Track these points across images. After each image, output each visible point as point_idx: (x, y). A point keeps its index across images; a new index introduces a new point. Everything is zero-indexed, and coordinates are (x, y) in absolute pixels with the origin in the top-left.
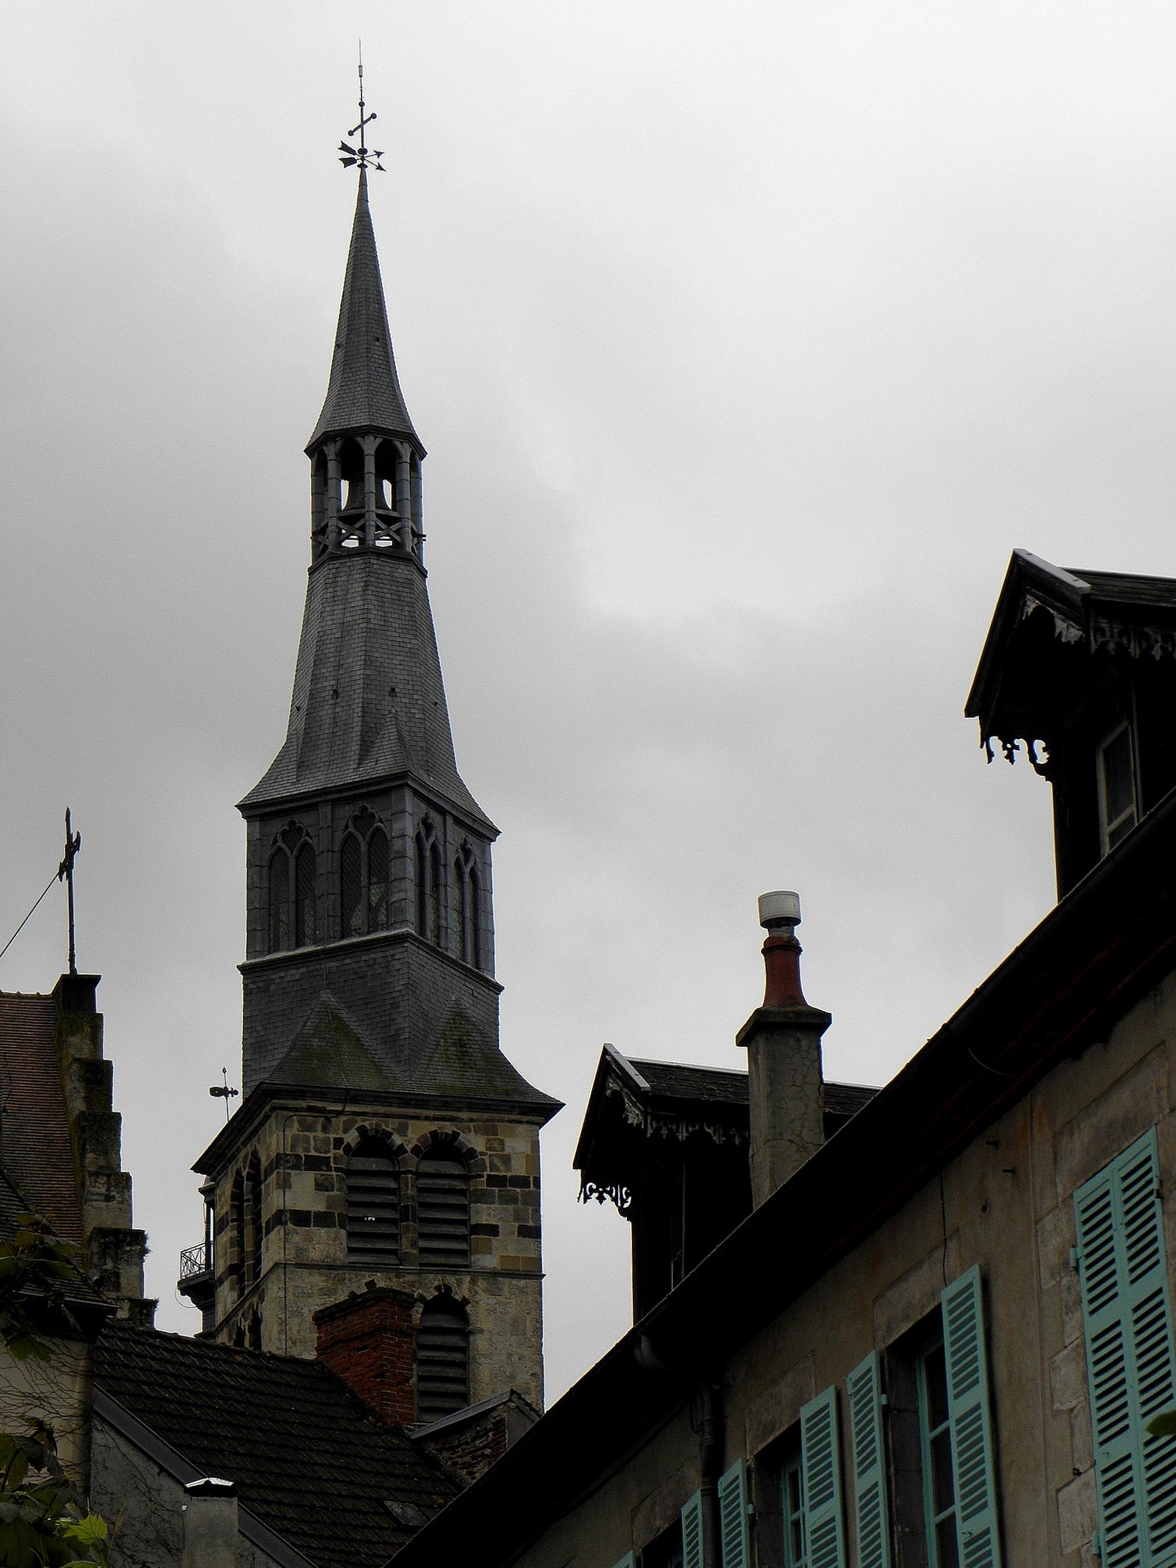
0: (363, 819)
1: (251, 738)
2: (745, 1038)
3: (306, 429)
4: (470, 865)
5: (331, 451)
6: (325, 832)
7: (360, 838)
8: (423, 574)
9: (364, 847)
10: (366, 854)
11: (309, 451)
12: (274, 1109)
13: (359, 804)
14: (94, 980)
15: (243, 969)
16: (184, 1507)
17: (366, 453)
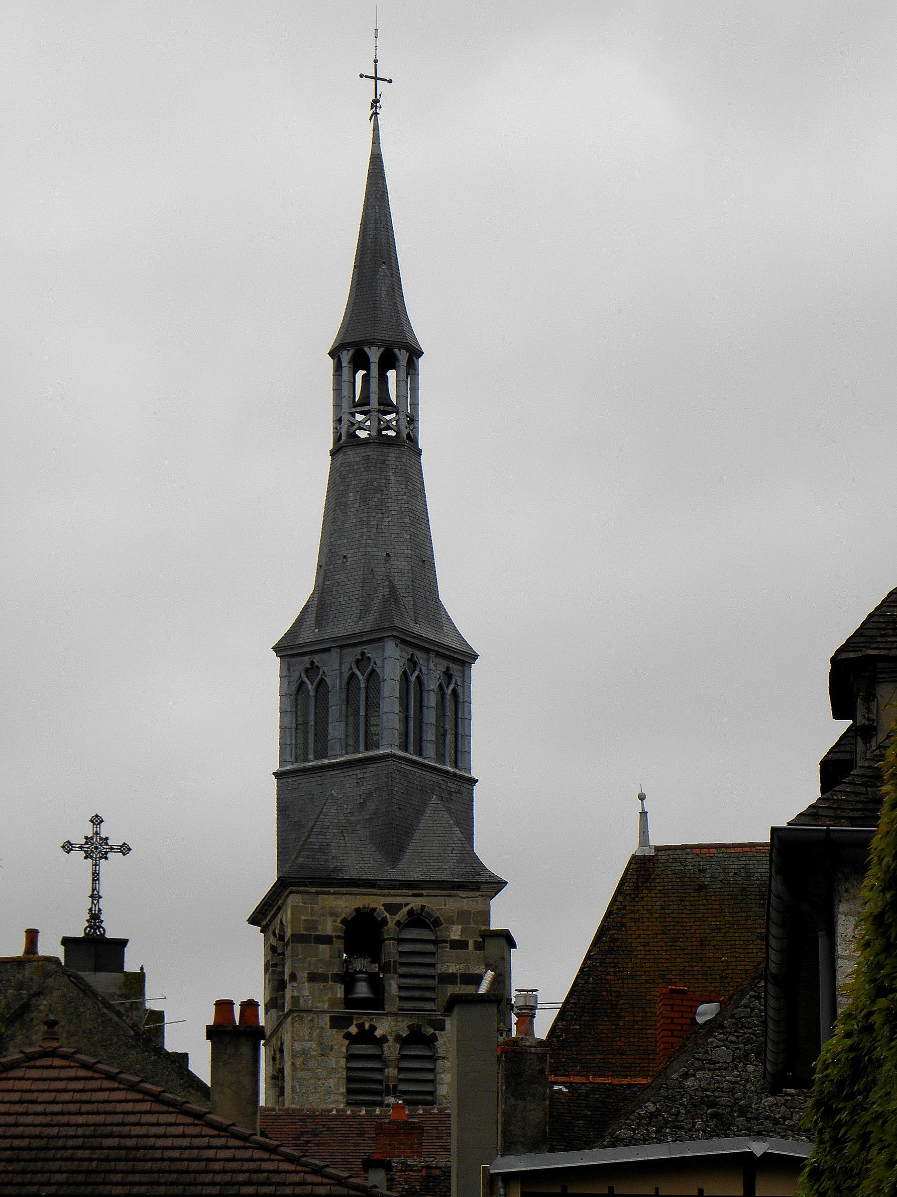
0: (362, 661)
1: (288, 584)
2: (838, 714)
3: (330, 338)
4: (452, 687)
5: (346, 356)
6: (334, 669)
7: (360, 677)
8: (419, 453)
9: (363, 685)
10: (374, 678)
11: (332, 354)
12: (290, 893)
13: (358, 650)
14: (123, 943)
15: (276, 774)
16: (706, 1012)
17: (375, 344)
